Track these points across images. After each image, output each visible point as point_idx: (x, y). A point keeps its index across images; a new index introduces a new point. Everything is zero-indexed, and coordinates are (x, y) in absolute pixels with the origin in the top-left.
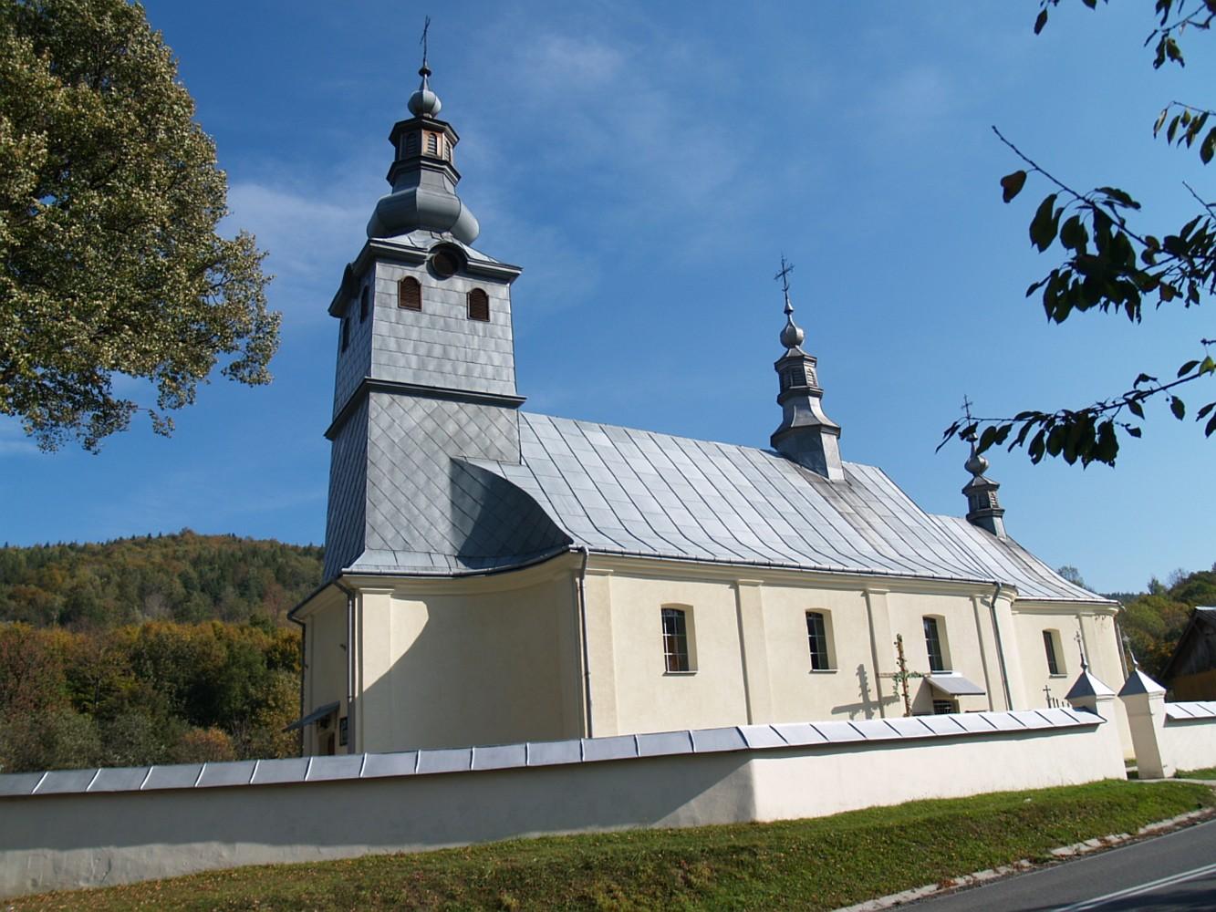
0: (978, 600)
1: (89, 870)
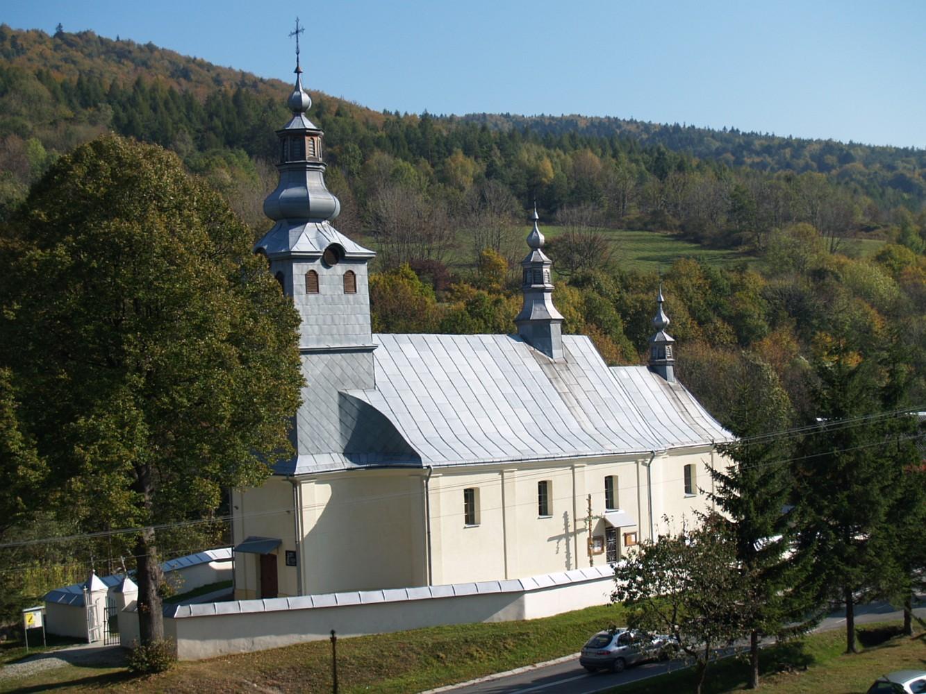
0: (640, 463)
1: (244, 645)
